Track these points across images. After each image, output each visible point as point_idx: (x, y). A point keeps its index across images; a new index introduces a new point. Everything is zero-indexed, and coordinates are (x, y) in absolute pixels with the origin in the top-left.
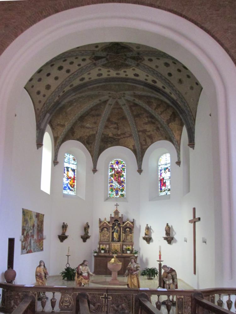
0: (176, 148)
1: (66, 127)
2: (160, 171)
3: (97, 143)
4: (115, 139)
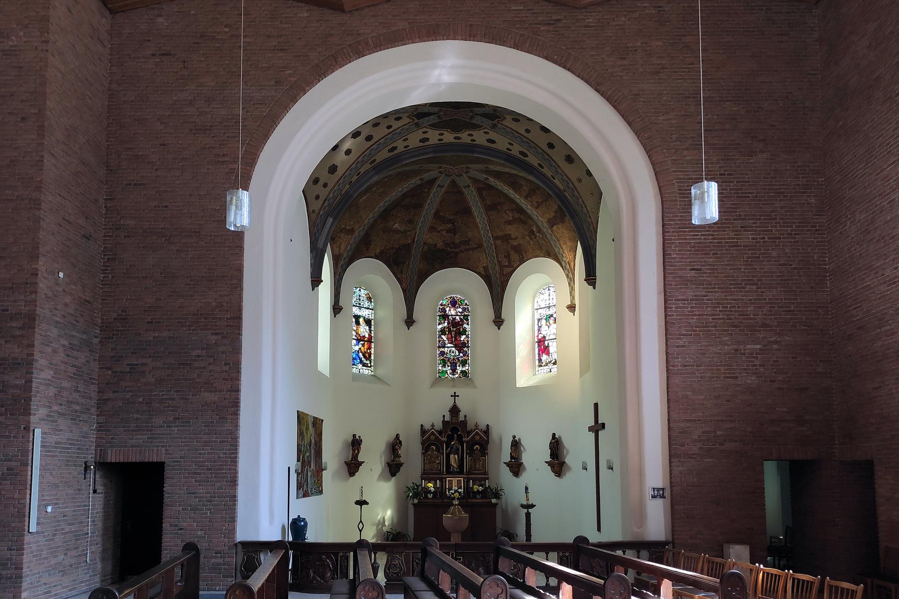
1: (356, 234)
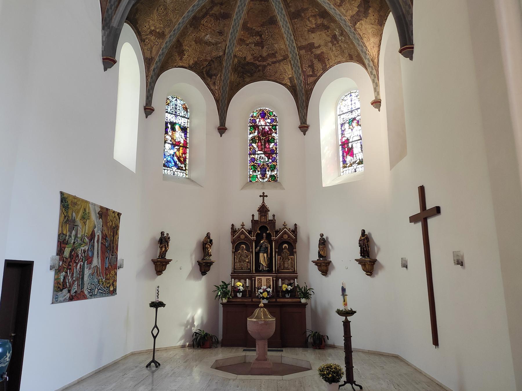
0: (371, 74)
1: (167, 39)
2: (342, 126)
3: (227, 74)
4: (257, 67)
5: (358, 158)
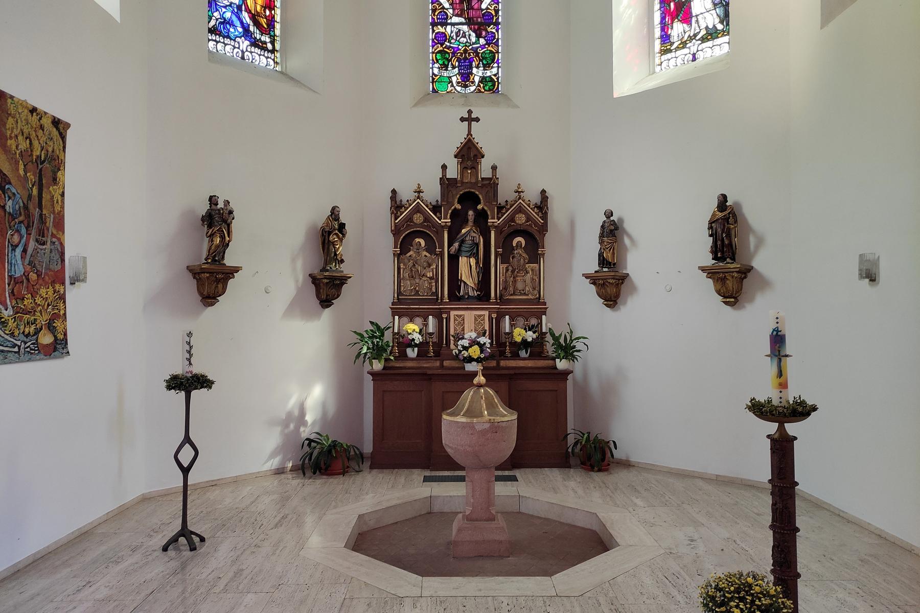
5: (703, 26)
